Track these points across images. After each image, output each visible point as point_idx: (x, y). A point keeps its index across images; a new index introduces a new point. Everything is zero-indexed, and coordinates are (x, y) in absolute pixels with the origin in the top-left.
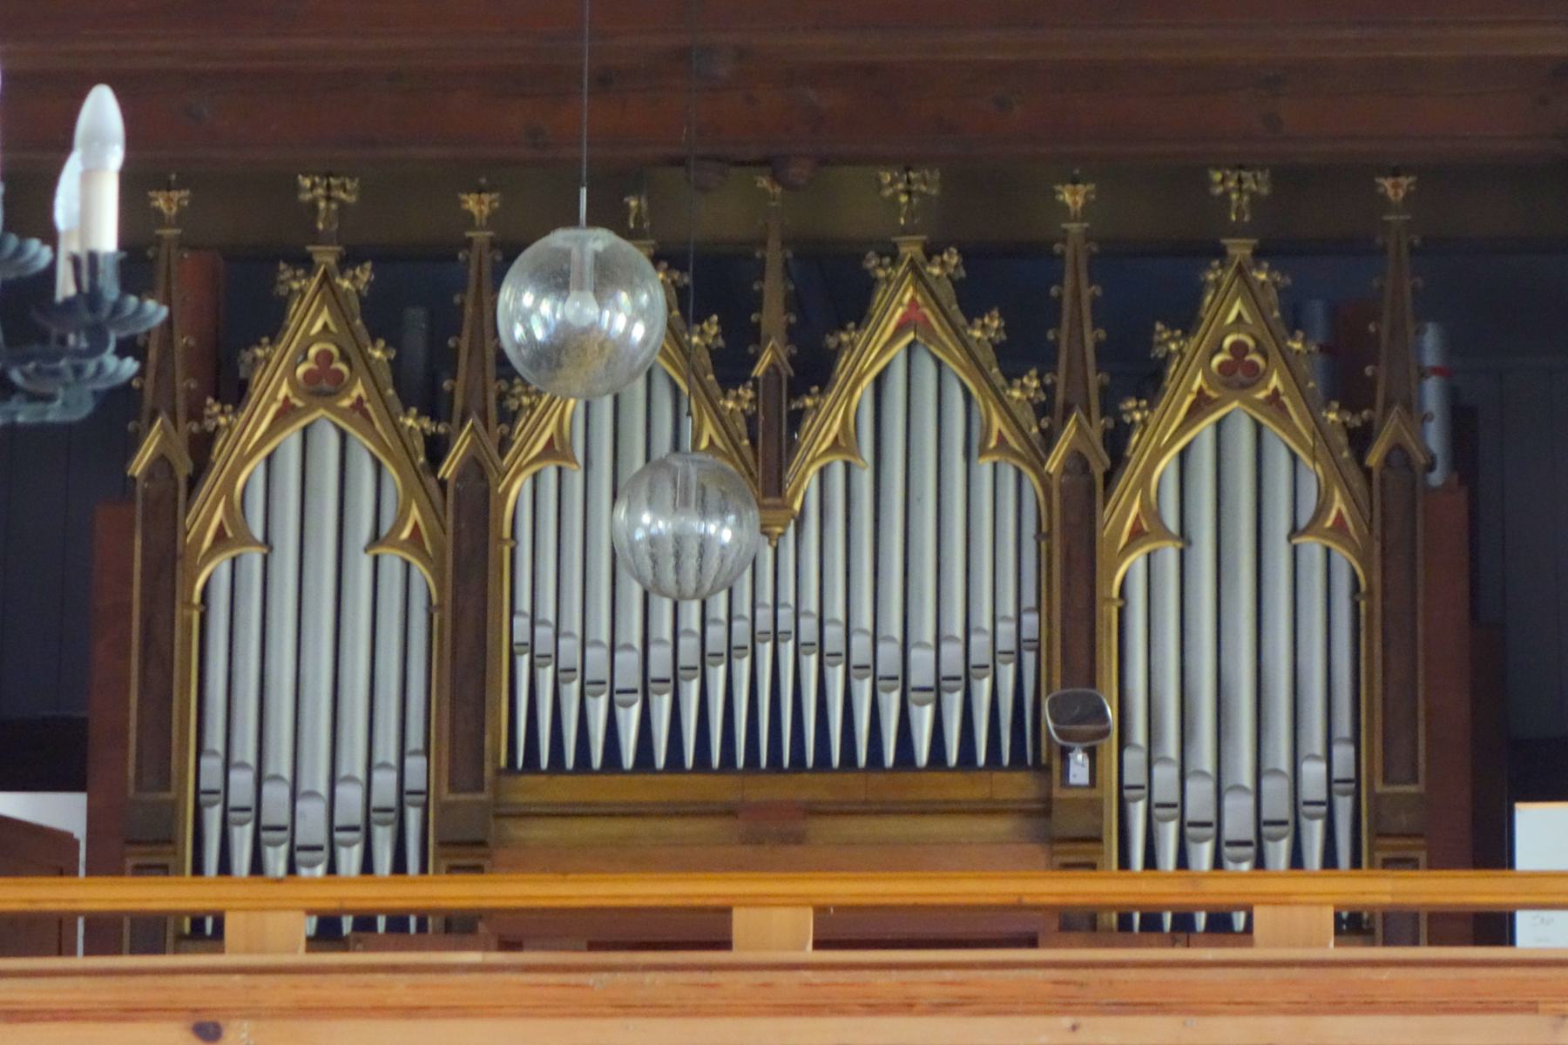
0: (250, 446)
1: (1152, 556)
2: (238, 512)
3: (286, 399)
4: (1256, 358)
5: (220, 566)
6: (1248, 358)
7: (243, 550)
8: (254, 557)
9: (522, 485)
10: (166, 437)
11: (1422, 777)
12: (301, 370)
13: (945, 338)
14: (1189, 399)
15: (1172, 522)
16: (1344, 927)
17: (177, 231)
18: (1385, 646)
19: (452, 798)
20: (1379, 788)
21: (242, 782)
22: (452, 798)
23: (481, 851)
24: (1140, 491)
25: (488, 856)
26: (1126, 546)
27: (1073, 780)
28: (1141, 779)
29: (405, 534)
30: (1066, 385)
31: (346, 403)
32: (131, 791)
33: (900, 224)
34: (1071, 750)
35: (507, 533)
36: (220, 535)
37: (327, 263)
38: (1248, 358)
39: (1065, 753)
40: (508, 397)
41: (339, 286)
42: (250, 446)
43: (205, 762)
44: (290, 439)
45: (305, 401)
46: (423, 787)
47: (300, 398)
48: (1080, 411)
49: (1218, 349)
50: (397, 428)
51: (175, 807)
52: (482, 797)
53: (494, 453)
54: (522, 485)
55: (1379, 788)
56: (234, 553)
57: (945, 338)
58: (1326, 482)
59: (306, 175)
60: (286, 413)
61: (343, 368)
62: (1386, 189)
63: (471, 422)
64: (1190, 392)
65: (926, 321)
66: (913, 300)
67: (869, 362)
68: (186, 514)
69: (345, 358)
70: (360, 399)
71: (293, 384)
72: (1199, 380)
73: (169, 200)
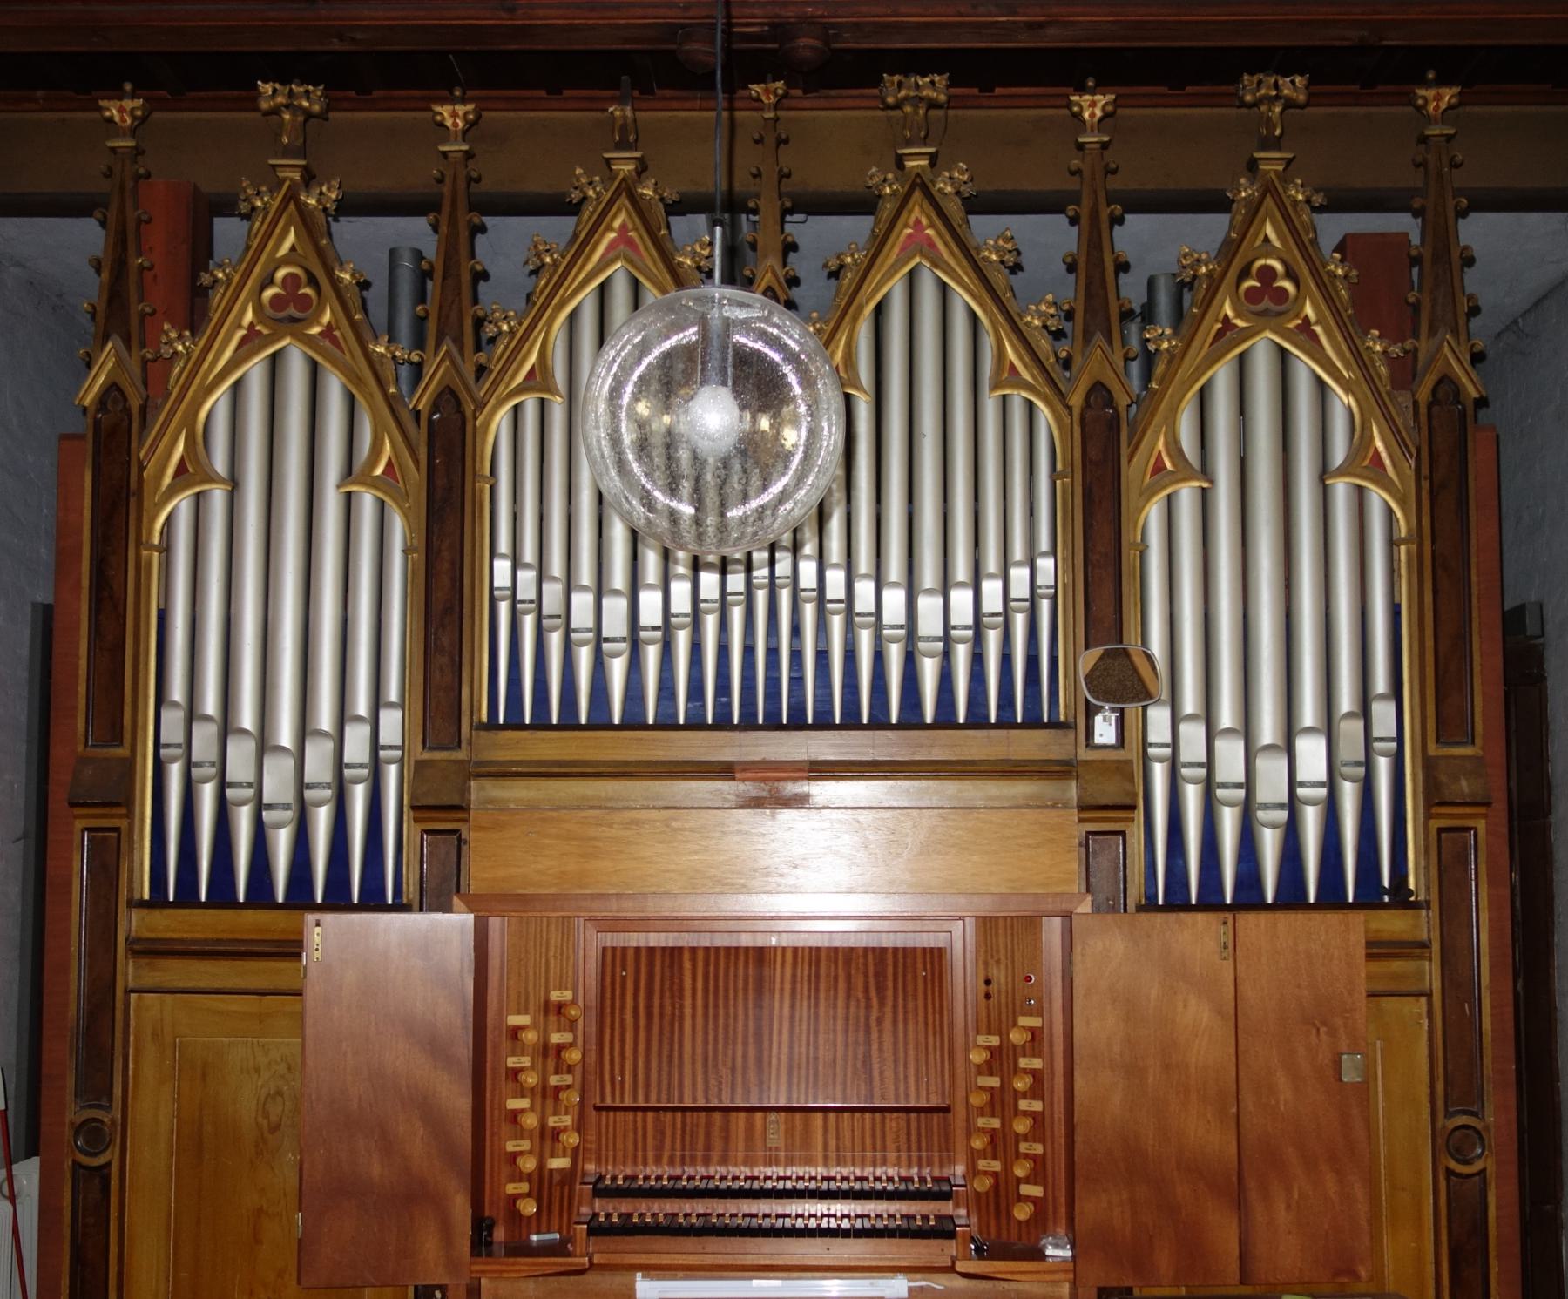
0: (211, 377)
1: (1173, 498)
2: (199, 444)
3: (252, 325)
4: (1288, 285)
5: (182, 504)
6: (1276, 285)
7: (206, 487)
8: (218, 496)
9: (502, 418)
10: (119, 363)
11: (1478, 740)
12: (269, 293)
13: (952, 262)
14: (240, 333)
15: (220, 464)
16: (1386, 899)
17: (131, 143)
18: (1435, 592)
19: (427, 756)
20: (1433, 749)
21: (204, 739)
22: (427, 756)
23: (460, 815)
24: (1164, 429)
25: (466, 821)
26: (170, 486)
27: (1098, 740)
28: (179, 738)
29: (379, 471)
30: (1085, 311)
31: (315, 330)
32: (80, 748)
33: (1273, 134)
34: (1100, 709)
35: (487, 472)
36: (181, 469)
37: (292, 180)
38: (1276, 285)
39: (1090, 712)
40: (486, 323)
41: (307, 205)
42: (211, 377)
43: (165, 714)
44: (255, 370)
45: (271, 328)
46: (399, 743)
47: (265, 325)
48: (452, 345)
49: (269, 281)
50: (368, 355)
51: (128, 768)
52: (461, 755)
53: (471, 380)
54: (502, 418)
55: (1433, 749)
56: (197, 489)
57: (952, 262)
58: (1362, 414)
59: (265, 81)
60: (251, 343)
61: (1288, 285)
62: (444, 118)
63: (445, 348)
64: (240, 326)
65: (932, 245)
66: (623, 226)
67: (570, 290)
68: (140, 446)
69: (1290, 274)
70: (329, 327)
71: (259, 309)
72: (249, 316)
73: (121, 110)
